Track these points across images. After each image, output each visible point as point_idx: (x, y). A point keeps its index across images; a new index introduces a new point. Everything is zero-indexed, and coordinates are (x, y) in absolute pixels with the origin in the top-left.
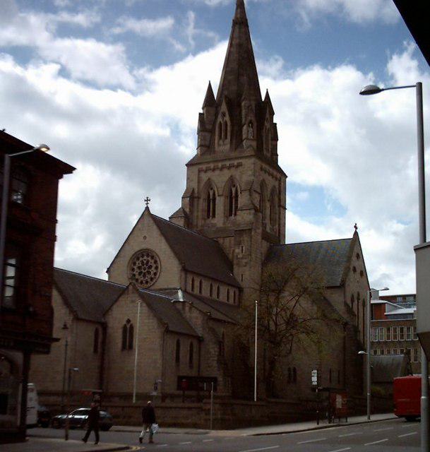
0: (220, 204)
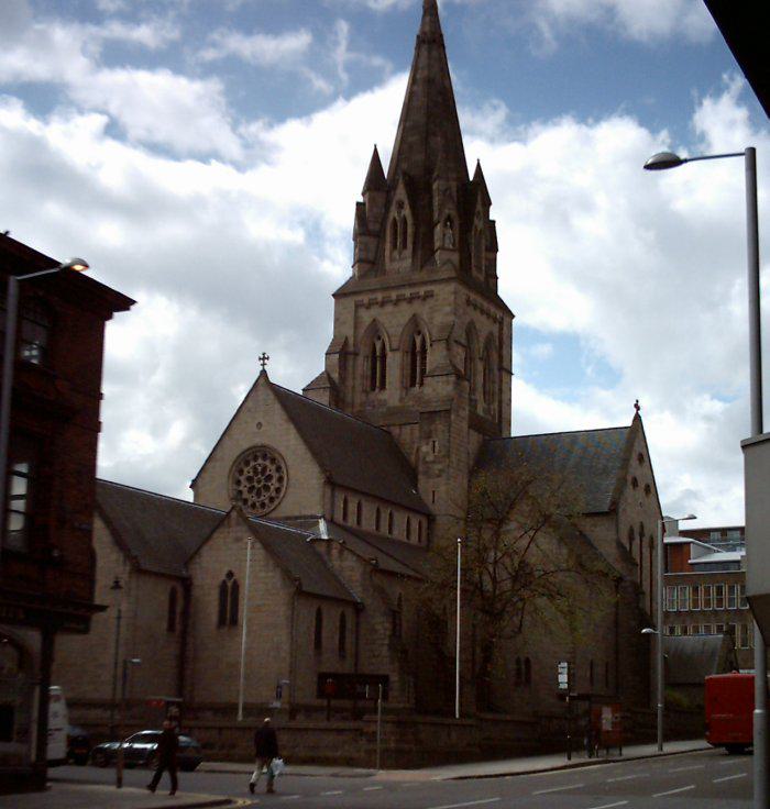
0: (395, 364)
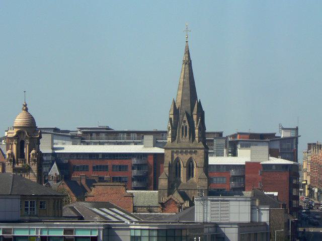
0: (183, 172)
